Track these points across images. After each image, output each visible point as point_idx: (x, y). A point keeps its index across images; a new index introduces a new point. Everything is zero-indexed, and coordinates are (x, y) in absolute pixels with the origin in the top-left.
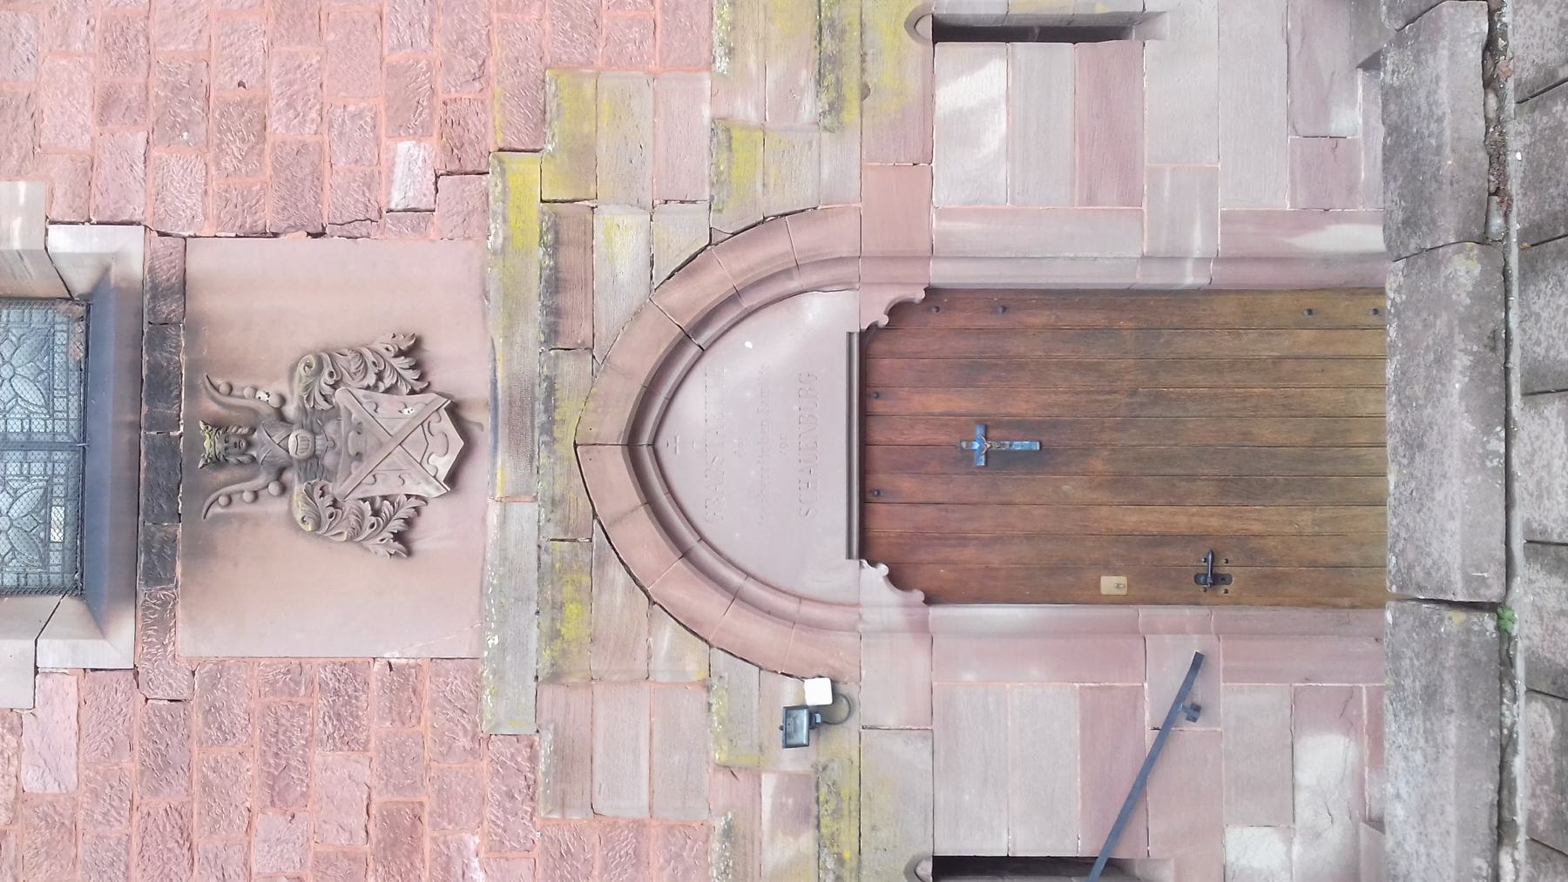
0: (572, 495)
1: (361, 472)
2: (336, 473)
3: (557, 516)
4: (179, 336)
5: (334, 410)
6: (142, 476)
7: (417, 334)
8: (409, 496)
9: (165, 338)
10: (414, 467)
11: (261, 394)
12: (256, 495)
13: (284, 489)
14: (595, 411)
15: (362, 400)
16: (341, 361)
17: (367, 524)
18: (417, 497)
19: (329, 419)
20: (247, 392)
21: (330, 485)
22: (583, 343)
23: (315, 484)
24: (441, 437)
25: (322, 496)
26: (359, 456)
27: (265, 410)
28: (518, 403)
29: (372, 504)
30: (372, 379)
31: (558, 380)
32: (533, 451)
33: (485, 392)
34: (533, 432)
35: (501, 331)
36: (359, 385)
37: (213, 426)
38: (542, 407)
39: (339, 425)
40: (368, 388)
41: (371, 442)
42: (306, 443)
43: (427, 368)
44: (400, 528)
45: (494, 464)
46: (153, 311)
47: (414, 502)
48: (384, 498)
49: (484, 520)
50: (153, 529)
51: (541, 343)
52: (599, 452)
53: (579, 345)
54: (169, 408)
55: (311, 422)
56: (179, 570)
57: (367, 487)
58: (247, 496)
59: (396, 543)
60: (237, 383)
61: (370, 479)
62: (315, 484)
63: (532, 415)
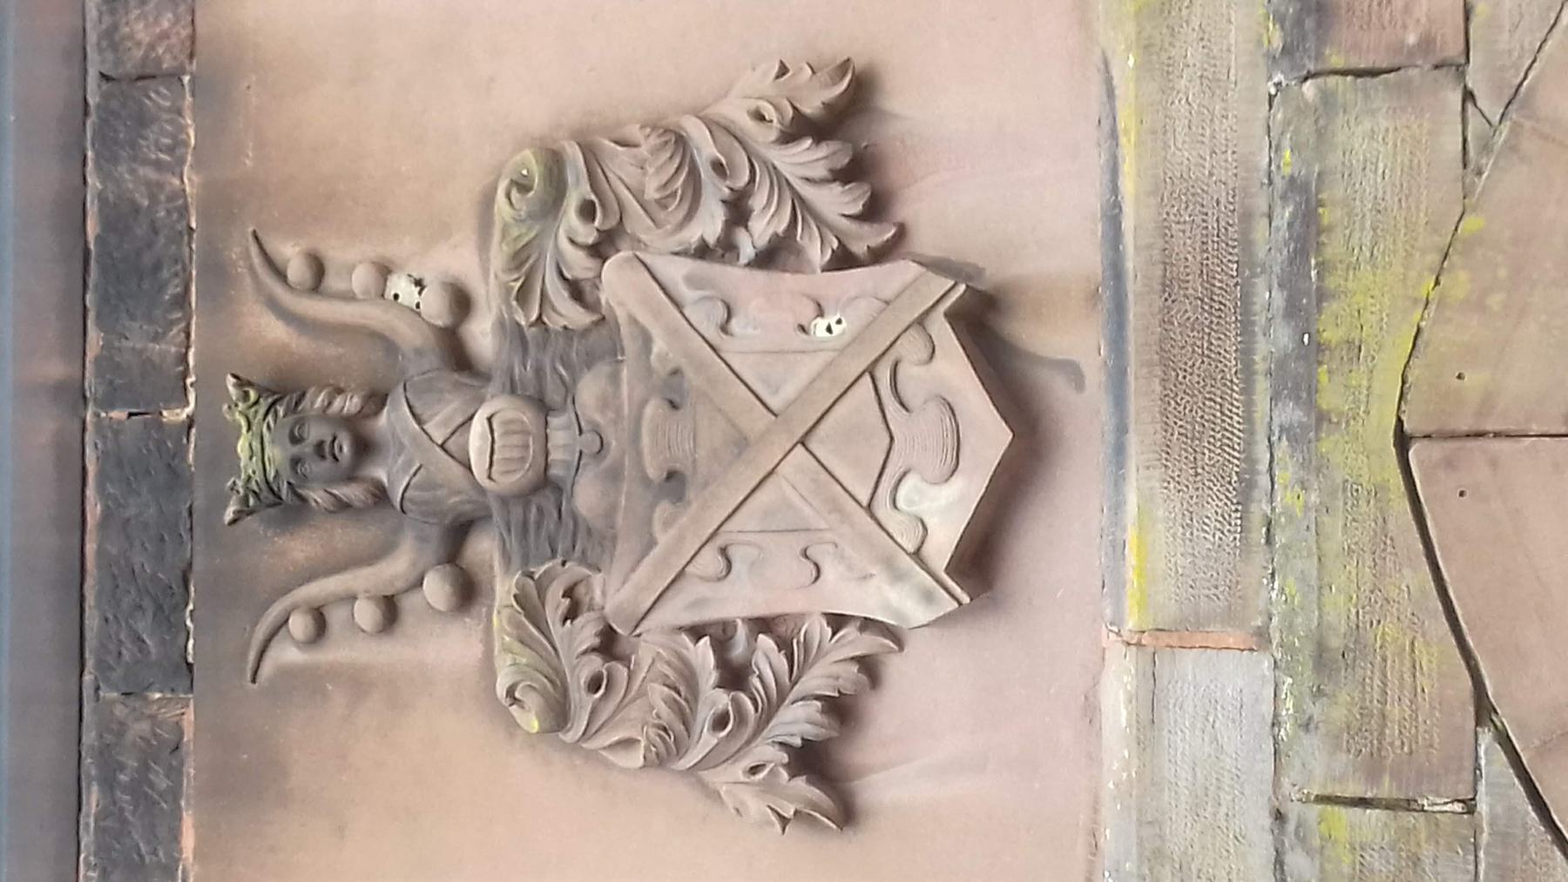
0: (1390, 628)
1: (680, 539)
2: (614, 539)
3: (1338, 711)
4: (180, 113)
5: (604, 331)
6: (91, 548)
7: (859, 63)
8: (837, 621)
9: (143, 120)
10: (845, 517)
11: (400, 285)
12: (390, 610)
13: (468, 592)
14: (1477, 304)
15: (686, 293)
16: (620, 165)
17: (705, 715)
18: (867, 624)
19: (590, 361)
20: (361, 278)
21: (597, 579)
22: (1426, 43)
23: (549, 576)
24: (934, 412)
25: (571, 614)
26: (674, 483)
27: (409, 335)
28: (1196, 286)
29: (722, 645)
30: (710, 223)
31: (1335, 191)
32: (1250, 461)
33: (1090, 259)
34: (1248, 390)
35: (1130, 28)
36: (674, 243)
37: (263, 391)
38: (1279, 299)
39: (615, 378)
40: (703, 251)
41: (712, 434)
42: (516, 440)
43: (894, 175)
44: (811, 732)
45: (1118, 507)
46: (112, 39)
47: (855, 642)
48: (762, 625)
49: (1090, 710)
50: (120, 711)
51: (1273, 61)
52: (1494, 463)
53: (1411, 53)
54: (156, 338)
55: (539, 371)
56: (188, 841)
57: (704, 590)
58: (366, 614)
59: (800, 783)
60: (336, 253)
61: (710, 561)
62: (549, 576)
63: (1246, 327)
